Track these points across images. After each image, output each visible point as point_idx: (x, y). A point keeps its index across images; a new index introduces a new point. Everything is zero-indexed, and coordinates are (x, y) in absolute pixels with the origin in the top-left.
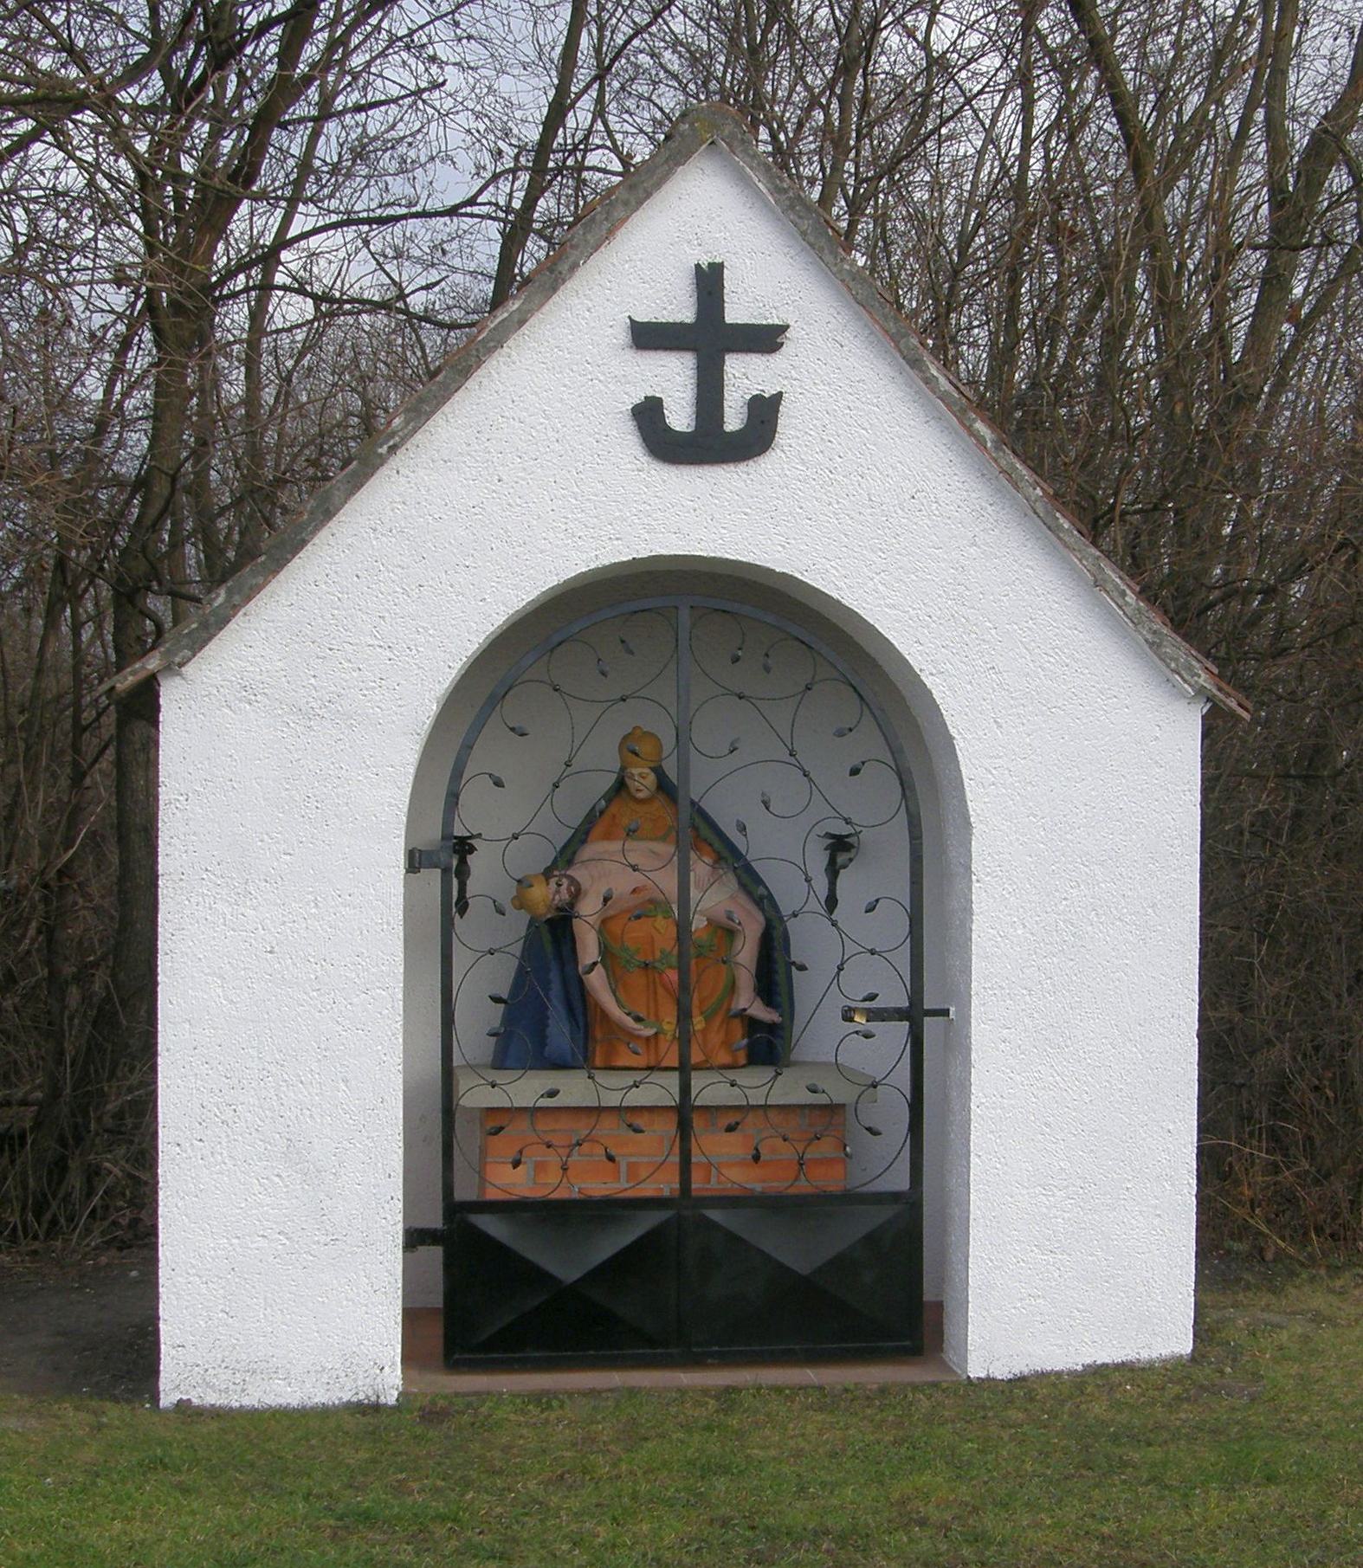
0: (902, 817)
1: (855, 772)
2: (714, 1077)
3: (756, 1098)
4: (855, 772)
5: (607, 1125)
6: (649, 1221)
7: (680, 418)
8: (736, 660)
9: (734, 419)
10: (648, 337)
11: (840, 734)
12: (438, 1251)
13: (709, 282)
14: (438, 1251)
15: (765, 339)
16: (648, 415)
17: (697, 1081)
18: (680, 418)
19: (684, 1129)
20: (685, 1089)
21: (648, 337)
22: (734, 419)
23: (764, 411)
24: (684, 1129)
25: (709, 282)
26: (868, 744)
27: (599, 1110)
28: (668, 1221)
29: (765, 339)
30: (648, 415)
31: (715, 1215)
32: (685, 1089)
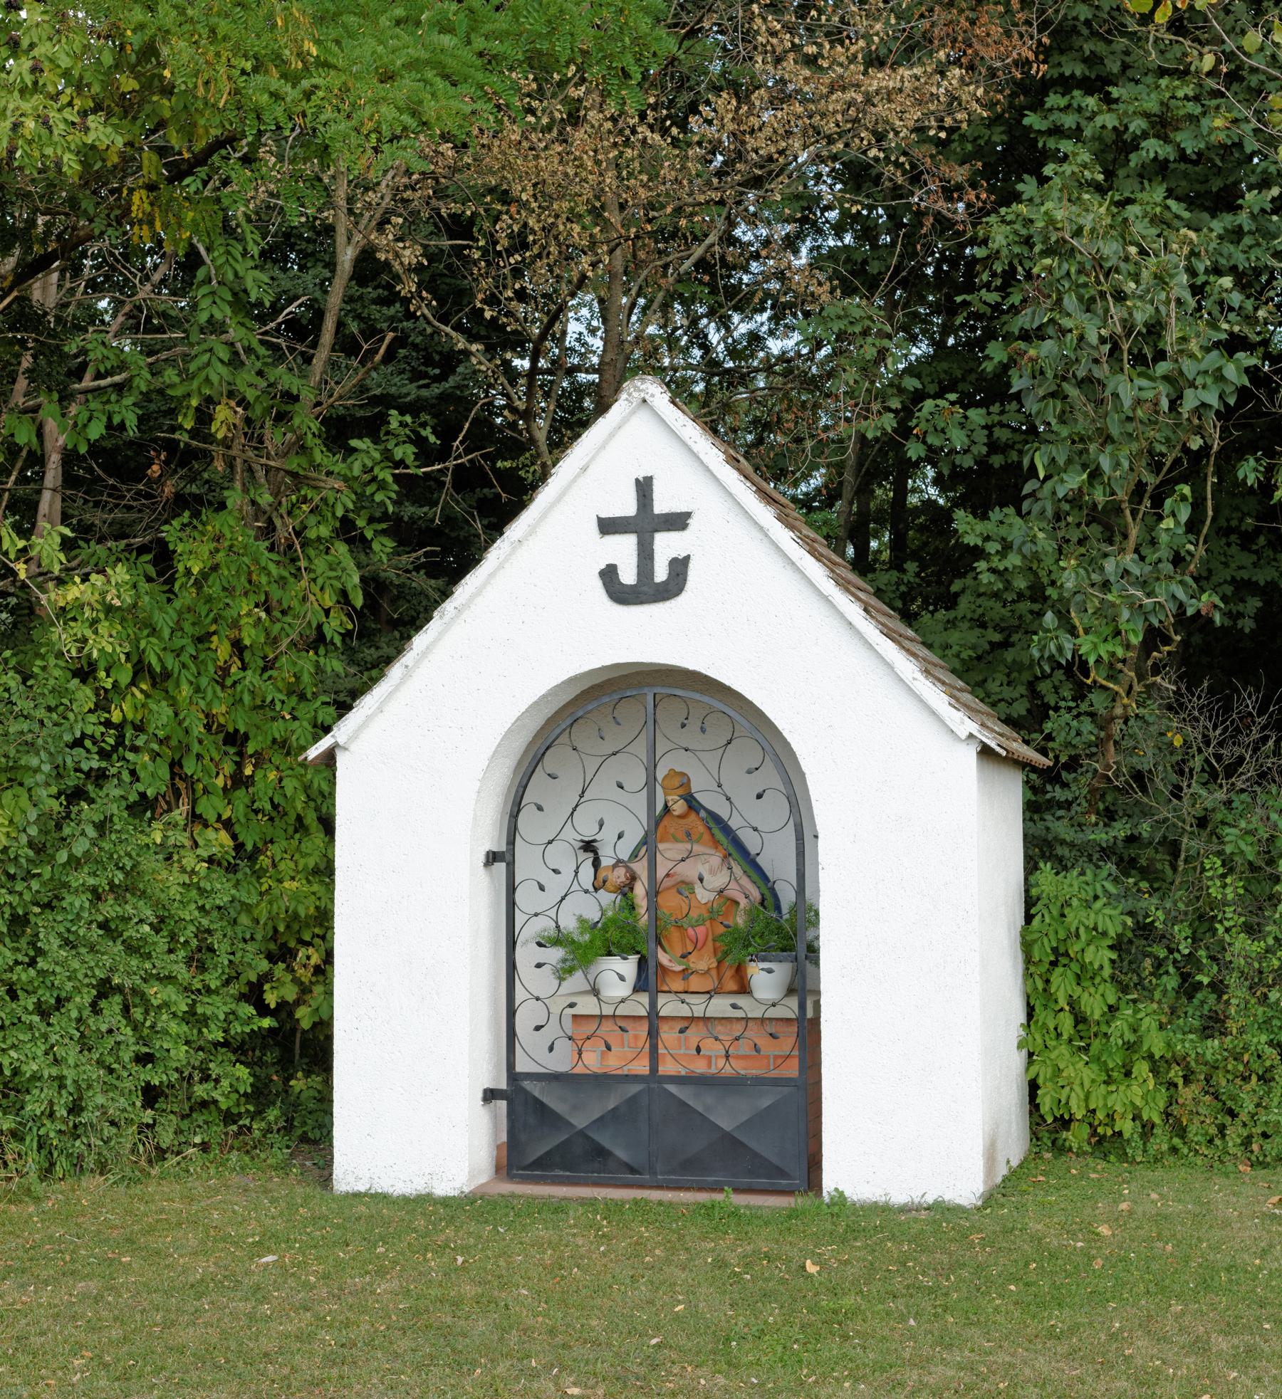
0: (790, 832)
1: (759, 796)
2: (672, 997)
3: (698, 1012)
4: (759, 796)
5: (608, 1027)
6: (635, 1089)
7: (628, 576)
8: (683, 726)
9: (661, 573)
10: (608, 526)
11: (749, 772)
12: (503, 1104)
13: (644, 488)
14: (503, 1104)
15: (678, 522)
16: (609, 574)
17: (662, 999)
18: (628, 576)
19: (653, 1034)
20: (653, 1004)
21: (608, 526)
22: (661, 573)
23: (680, 567)
24: (653, 1034)
25: (644, 488)
26: (769, 777)
27: (601, 1017)
28: (640, 1093)
29: (678, 522)
30: (609, 574)
31: (672, 1088)
32: (653, 1004)
